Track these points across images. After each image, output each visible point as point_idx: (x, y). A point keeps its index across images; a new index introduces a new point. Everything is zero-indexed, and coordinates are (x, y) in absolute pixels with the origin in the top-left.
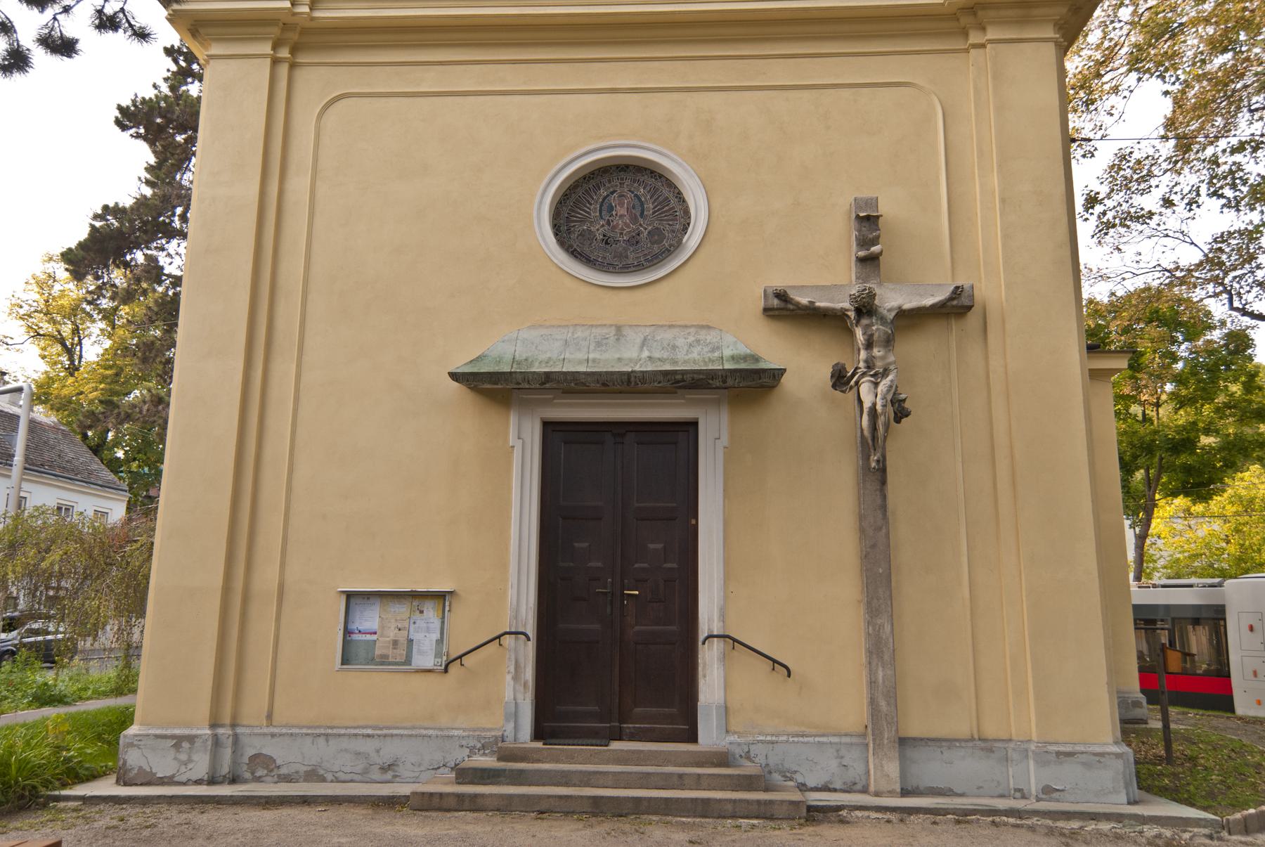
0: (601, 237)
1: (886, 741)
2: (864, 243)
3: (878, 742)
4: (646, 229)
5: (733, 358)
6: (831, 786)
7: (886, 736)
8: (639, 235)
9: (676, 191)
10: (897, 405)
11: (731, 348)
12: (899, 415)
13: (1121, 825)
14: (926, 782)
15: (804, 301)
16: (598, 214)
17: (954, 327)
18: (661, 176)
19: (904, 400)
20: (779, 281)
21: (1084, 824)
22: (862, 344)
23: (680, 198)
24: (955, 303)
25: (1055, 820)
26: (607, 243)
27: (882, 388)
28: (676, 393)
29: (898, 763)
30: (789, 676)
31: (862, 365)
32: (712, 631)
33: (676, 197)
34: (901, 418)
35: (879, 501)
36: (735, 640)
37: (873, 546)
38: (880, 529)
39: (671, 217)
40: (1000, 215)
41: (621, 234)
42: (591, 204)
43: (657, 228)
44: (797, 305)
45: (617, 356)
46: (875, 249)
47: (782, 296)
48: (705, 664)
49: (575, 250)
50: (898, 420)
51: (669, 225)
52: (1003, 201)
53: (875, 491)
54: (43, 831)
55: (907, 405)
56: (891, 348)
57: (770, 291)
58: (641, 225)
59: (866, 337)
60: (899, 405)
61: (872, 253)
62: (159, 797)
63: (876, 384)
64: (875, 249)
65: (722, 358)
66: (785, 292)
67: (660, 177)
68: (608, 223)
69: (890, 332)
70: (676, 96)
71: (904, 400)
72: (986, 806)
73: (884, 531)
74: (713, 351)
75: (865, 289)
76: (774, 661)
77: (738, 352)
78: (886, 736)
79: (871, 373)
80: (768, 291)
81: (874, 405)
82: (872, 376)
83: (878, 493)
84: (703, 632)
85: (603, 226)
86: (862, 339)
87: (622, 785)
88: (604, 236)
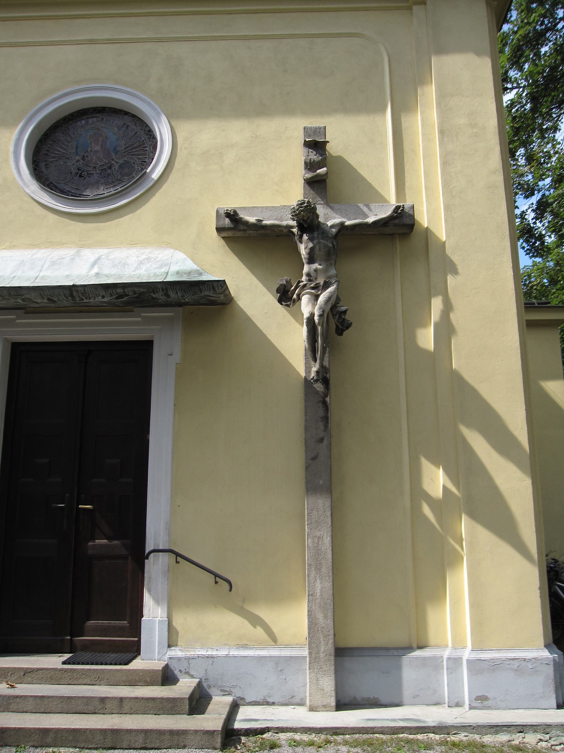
0: (76, 171)
1: (322, 655)
2: (310, 166)
3: (313, 655)
4: (117, 163)
5: (178, 273)
6: (271, 700)
7: (322, 649)
8: (110, 168)
9: (148, 129)
10: (337, 316)
11: (178, 265)
12: (340, 327)
13: (547, 736)
14: (364, 693)
15: (252, 219)
16: (74, 151)
17: (398, 248)
18: (126, 113)
19: (345, 312)
20: (230, 204)
21: (511, 738)
22: (305, 258)
23: (151, 135)
24: (397, 221)
25: (482, 734)
26: (81, 176)
27: (322, 298)
28: (133, 311)
29: (333, 677)
30: (230, 590)
31: (304, 278)
32: (159, 546)
33: (147, 134)
34: (343, 330)
35: (321, 413)
36: (177, 555)
37: (314, 458)
38: (321, 440)
39: (141, 152)
40: (440, 144)
41: (95, 167)
42: (68, 142)
43: (128, 162)
44: (246, 223)
45: (67, 273)
46: (323, 170)
47: (233, 216)
48: (150, 578)
49: (51, 183)
50: (340, 331)
51: (139, 159)
52: (442, 132)
53: (319, 402)
54: (310, 747)
55: (347, 317)
56: (333, 262)
57: (222, 212)
58: (113, 159)
59: (308, 251)
60: (340, 317)
61: (318, 175)
62: (403, 728)
63: (317, 297)
64: (323, 170)
65: (167, 273)
66: (235, 212)
67: (120, 112)
68: (83, 158)
69: (330, 245)
70: (148, 46)
71: (345, 312)
72: (416, 720)
73: (325, 442)
74: (161, 267)
75: (304, 203)
76: (216, 575)
77: (185, 267)
78: (322, 649)
79: (312, 285)
80: (220, 212)
81: (312, 315)
82: (313, 288)
83: (320, 404)
84: (149, 546)
85: (78, 161)
86: (304, 253)
87: (42, 710)
88: (79, 170)
